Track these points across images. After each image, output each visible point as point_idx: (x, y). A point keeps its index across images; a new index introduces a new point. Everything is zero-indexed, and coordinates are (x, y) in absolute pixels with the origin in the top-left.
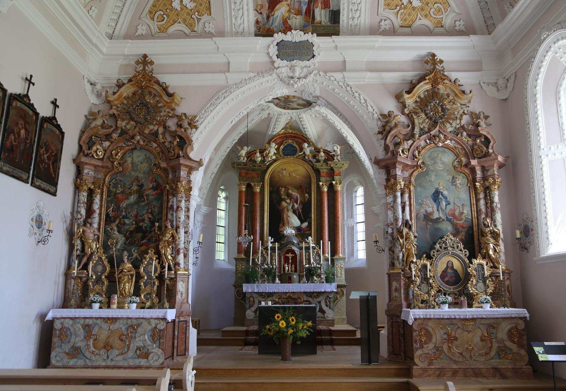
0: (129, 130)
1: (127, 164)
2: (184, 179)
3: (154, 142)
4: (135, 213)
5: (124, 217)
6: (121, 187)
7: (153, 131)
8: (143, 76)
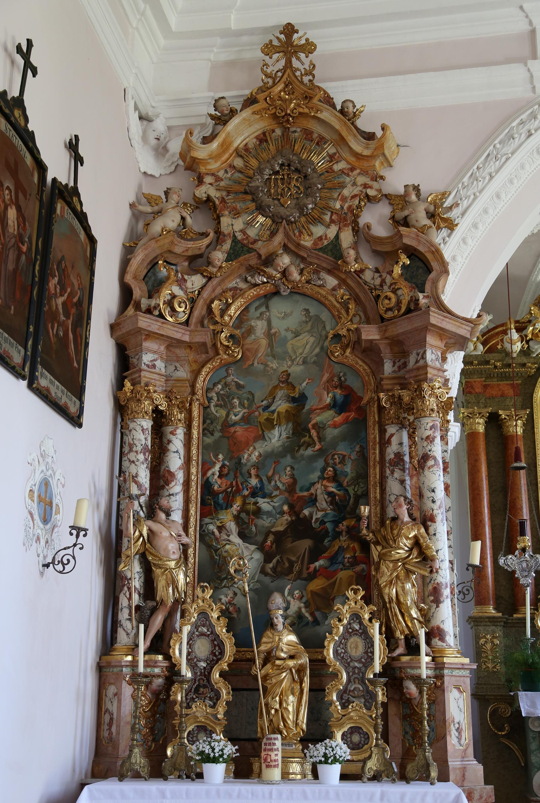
0: (255, 241)
1: (253, 337)
2: (435, 372)
3: (330, 272)
4: (286, 479)
5: (254, 494)
6: (242, 405)
7: (326, 242)
8: (286, 86)
